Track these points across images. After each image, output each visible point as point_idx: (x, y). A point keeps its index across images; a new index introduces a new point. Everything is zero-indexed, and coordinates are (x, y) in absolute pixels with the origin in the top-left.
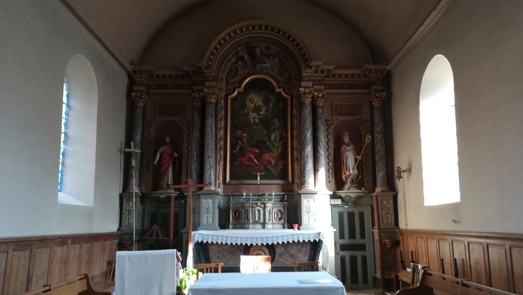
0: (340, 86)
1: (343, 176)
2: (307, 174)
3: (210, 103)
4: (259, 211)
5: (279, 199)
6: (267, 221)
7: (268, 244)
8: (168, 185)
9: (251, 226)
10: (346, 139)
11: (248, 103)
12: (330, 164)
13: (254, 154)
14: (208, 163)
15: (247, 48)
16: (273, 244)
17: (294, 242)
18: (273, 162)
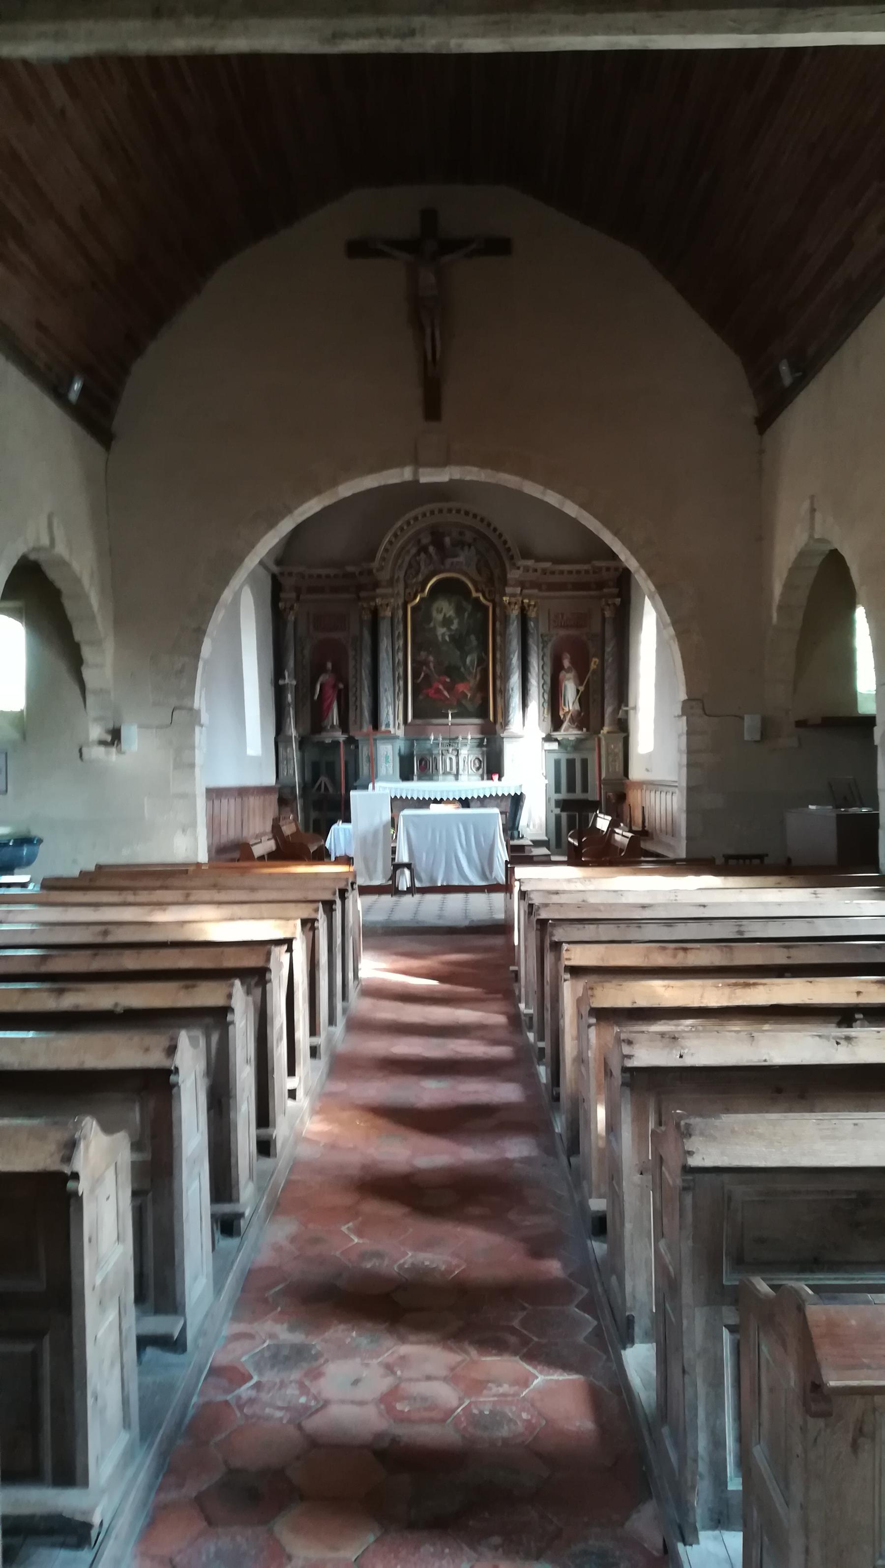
0: (561, 587)
1: (561, 714)
2: (512, 713)
3: (384, 618)
4: (451, 759)
5: (476, 744)
6: (461, 771)
7: (460, 799)
8: (333, 726)
9: (441, 777)
10: (566, 663)
11: (434, 613)
12: (546, 696)
13: (444, 684)
14: (385, 698)
15: (433, 533)
16: (467, 798)
17: (491, 795)
18: (469, 695)
